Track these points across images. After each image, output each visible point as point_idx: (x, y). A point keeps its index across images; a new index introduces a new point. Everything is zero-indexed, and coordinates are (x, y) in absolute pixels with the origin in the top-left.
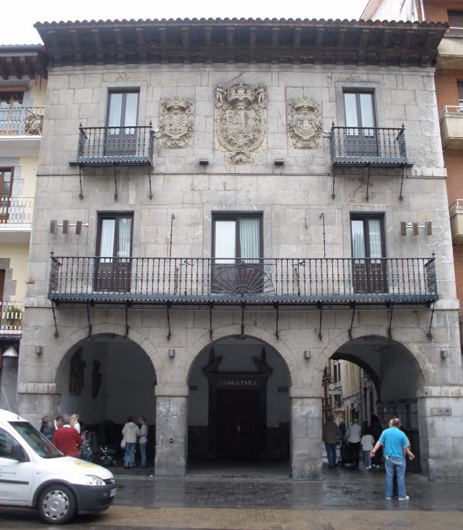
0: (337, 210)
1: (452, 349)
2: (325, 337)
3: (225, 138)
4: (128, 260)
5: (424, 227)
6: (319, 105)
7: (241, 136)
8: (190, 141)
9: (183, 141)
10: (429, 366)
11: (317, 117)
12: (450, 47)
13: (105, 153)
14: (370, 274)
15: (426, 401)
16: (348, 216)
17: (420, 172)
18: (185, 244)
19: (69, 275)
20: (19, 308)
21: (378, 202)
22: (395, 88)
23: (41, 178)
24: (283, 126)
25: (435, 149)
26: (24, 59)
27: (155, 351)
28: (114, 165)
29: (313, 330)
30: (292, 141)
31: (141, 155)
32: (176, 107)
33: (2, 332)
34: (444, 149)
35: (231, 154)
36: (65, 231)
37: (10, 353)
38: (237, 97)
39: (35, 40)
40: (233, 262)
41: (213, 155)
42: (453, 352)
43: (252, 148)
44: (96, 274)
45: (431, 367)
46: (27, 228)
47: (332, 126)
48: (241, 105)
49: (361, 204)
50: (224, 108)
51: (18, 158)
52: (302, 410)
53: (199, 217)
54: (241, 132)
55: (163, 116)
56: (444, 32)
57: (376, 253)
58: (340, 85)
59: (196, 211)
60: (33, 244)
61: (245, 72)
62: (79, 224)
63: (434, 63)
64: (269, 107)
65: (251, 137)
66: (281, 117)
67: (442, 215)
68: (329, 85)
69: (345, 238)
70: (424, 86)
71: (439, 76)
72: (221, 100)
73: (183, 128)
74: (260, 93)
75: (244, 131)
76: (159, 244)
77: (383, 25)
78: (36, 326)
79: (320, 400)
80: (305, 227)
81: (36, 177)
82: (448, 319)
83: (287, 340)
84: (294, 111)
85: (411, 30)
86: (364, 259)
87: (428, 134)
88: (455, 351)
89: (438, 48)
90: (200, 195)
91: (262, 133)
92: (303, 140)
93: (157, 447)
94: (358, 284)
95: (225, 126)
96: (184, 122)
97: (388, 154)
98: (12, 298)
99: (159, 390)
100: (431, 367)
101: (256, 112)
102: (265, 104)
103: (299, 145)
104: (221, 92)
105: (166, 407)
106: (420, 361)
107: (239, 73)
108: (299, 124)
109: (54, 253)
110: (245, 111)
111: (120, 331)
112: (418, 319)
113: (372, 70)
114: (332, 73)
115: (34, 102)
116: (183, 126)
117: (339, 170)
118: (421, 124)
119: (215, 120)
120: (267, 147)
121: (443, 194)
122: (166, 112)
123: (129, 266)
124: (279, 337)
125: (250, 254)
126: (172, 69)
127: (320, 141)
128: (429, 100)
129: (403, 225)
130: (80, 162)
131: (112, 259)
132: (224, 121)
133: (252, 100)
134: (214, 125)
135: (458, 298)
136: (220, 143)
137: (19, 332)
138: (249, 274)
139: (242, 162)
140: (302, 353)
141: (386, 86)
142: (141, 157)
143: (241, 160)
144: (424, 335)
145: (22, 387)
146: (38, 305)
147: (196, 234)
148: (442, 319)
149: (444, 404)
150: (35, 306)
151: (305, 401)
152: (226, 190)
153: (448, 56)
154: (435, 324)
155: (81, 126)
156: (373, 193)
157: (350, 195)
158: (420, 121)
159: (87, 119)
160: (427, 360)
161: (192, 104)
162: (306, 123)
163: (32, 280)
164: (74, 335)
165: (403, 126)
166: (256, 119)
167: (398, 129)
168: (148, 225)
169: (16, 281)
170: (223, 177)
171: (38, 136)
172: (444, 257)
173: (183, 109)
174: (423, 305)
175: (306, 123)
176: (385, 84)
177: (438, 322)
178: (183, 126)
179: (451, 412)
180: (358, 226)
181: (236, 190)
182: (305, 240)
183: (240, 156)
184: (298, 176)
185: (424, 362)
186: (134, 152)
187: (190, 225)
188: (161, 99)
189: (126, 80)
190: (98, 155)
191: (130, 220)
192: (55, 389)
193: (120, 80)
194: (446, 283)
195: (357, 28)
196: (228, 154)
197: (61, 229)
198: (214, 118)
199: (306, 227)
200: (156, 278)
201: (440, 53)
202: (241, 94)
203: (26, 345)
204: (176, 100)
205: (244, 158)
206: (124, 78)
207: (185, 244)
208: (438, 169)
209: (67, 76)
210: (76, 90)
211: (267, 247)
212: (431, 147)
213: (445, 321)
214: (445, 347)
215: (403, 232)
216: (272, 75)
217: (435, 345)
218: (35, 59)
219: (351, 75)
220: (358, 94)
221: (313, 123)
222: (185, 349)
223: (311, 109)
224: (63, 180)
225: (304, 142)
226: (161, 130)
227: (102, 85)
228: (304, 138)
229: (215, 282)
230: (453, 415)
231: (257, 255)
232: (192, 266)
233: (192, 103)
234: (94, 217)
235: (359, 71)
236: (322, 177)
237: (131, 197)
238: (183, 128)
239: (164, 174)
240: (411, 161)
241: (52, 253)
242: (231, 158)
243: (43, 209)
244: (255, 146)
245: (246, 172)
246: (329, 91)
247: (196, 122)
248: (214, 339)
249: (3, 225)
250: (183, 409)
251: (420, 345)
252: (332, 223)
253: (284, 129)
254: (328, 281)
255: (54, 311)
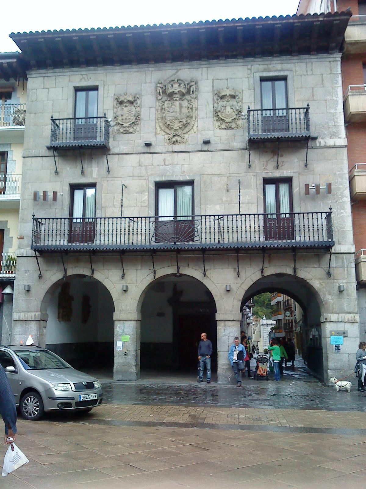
0: (252, 177)
1: (348, 284)
2: (242, 275)
3: (164, 124)
4: (94, 219)
5: (325, 187)
6: (240, 93)
7: (176, 122)
8: (137, 128)
9: (132, 127)
10: (327, 296)
11: (238, 103)
12: (355, 33)
13: (75, 138)
14: (279, 225)
15: (326, 325)
16: (261, 181)
17: (324, 143)
18: (135, 207)
19: (51, 231)
20: (13, 257)
21: (287, 169)
22: (306, 74)
23: (25, 159)
24: (211, 112)
25: (338, 123)
26: (6, 64)
27: (113, 287)
28: (81, 148)
29: (233, 269)
30: (217, 124)
31: (99, 140)
32: (125, 101)
33: (1, 275)
34: (346, 122)
35: (169, 137)
36: (45, 199)
37: (8, 290)
38: (173, 90)
39: (13, 48)
40: (172, 219)
41: (155, 138)
42: (350, 287)
43: (185, 131)
44: (70, 231)
45: (330, 299)
46: (17, 197)
47: (248, 109)
48: (177, 97)
49: (273, 171)
50: (163, 100)
51: (10, 144)
52: (225, 330)
53: (145, 186)
54: (176, 119)
55: (116, 108)
56: (348, 20)
57: (285, 209)
58: (258, 75)
59: (143, 182)
60: (22, 209)
61: (181, 69)
62: (55, 194)
63: (341, 50)
64: (199, 97)
65: (185, 122)
66: (209, 105)
67: (341, 177)
68: (249, 76)
69: (258, 199)
70: (331, 70)
71: (346, 59)
72: (161, 94)
73: (131, 118)
74: (192, 86)
75: (179, 118)
76: (115, 207)
77: (294, 19)
78: (26, 270)
79: (239, 323)
80: (226, 191)
81: (22, 158)
82: (345, 261)
83: (212, 277)
84: (219, 99)
85: (318, 21)
86: (289, 214)
87: (332, 111)
88: (351, 286)
89: (345, 35)
90: (146, 169)
91: (194, 119)
92: (226, 123)
93: (115, 358)
94: (268, 234)
95: (164, 115)
96: (132, 113)
97: (296, 130)
98: (10, 250)
99: (116, 316)
100: (330, 299)
101: (188, 101)
102: (196, 95)
103: (223, 126)
104: (160, 87)
105: (122, 329)
106: (321, 294)
107: (175, 71)
108: (222, 109)
109: (35, 215)
110: (180, 102)
111: (87, 272)
112: (319, 261)
113: (285, 60)
114: (252, 65)
115: (19, 100)
116: (132, 116)
117: (256, 145)
118: (326, 103)
119: (157, 110)
120: (198, 130)
121: (343, 160)
122: (118, 105)
123: (94, 224)
124: (206, 275)
125: (184, 212)
126: (123, 70)
127: (240, 122)
128: (335, 81)
129: (307, 186)
130: (52, 146)
131: (82, 219)
132: (163, 110)
133: (185, 93)
134: (156, 114)
135: (354, 244)
136: (161, 128)
137: (13, 275)
138: (185, 228)
139: (178, 142)
140: (225, 286)
141: (297, 73)
142: (99, 141)
143: (177, 141)
144: (325, 273)
145: (16, 316)
146: (27, 254)
147: (143, 199)
148: (340, 260)
149: (341, 327)
150: (25, 255)
151: (227, 323)
152: (166, 165)
153: (354, 42)
154: (333, 264)
155: (52, 117)
156: (283, 162)
157: (264, 164)
158: (326, 100)
159: (59, 112)
160: (327, 293)
161: (138, 98)
162: (228, 109)
163: (22, 236)
164: (54, 275)
165: (308, 105)
166: (189, 108)
167: (304, 108)
168: (107, 193)
169: (12, 237)
170: (163, 154)
171: (22, 127)
172: (342, 211)
173: (131, 102)
174: (322, 250)
175: (228, 109)
176: (296, 71)
177: (336, 263)
178: (132, 116)
179: (347, 334)
180: (271, 189)
181: (173, 164)
182: (227, 201)
183: (176, 138)
184: (222, 152)
185: (325, 295)
186: (96, 138)
187: (137, 193)
188: (114, 95)
189: (87, 80)
190: (66, 140)
191: (94, 189)
192: (40, 317)
193: (83, 80)
194: (344, 232)
195: (271, 24)
196: (167, 137)
197: (42, 197)
198: (156, 109)
199: (228, 191)
200: (115, 233)
201: (347, 39)
202: (176, 88)
203: (18, 285)
204: (125, 95)
205: (179, 139)
206: (86, 79)
207: (135, 207)
208: (340, 139)
209: (42, 78)
210: (50, 89)
211: (197, 207)
212: (334, 122)
213: (343, 262)
214: (343, 283)
215: (307, 192)
216: (202, 70)
217: (334, 281)
218: (14, 65)
219: (268, 66)
220: (274, 82)
221: (234, 108)
222: (135, 285)
223: (233, 97)
224: (42, 160)
225: (227, 124)
226: (115, 119)
227: (69, 84)
228: (227, 120)
229: (157, 236)
230: (348, 336)
231: (190, 213)
232: (137, 223)
233: (138, 97)
234: (67, 189)
235: (274, 62)
236: (241, 151)
237: (94, 171)
238: (131, 118)
239: (119, 154)
240: (317, 134)
241: (34, 216)
242: (169, 139)
243: (28, 183)
244: (188, 129)
245: (181, 150)
246: (249, 80)
247: (142, 112)
248: (156, 277)
249: (2, 196)
250: (134, 329)
251: (321, 281)
252: (248, 187)
253: (211, 114)
254: (246, 231)
255: (37, 259)
